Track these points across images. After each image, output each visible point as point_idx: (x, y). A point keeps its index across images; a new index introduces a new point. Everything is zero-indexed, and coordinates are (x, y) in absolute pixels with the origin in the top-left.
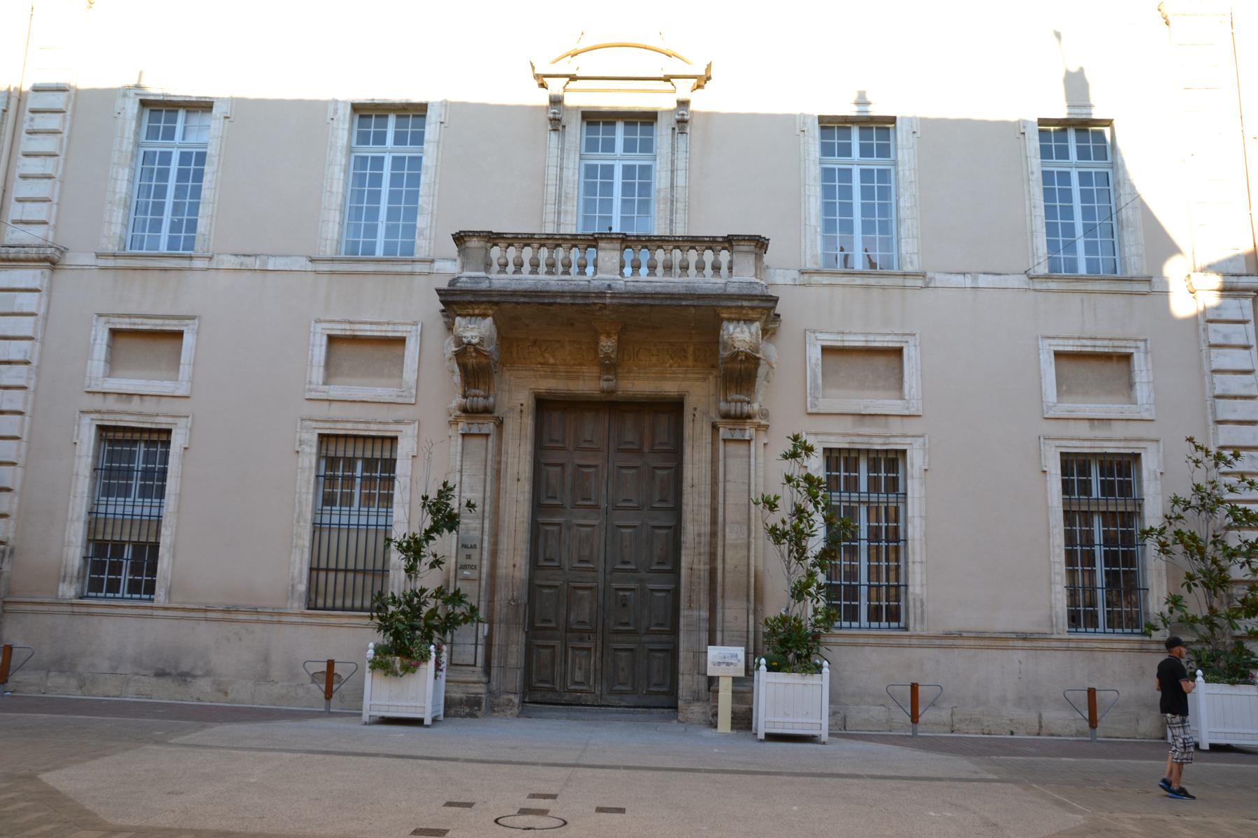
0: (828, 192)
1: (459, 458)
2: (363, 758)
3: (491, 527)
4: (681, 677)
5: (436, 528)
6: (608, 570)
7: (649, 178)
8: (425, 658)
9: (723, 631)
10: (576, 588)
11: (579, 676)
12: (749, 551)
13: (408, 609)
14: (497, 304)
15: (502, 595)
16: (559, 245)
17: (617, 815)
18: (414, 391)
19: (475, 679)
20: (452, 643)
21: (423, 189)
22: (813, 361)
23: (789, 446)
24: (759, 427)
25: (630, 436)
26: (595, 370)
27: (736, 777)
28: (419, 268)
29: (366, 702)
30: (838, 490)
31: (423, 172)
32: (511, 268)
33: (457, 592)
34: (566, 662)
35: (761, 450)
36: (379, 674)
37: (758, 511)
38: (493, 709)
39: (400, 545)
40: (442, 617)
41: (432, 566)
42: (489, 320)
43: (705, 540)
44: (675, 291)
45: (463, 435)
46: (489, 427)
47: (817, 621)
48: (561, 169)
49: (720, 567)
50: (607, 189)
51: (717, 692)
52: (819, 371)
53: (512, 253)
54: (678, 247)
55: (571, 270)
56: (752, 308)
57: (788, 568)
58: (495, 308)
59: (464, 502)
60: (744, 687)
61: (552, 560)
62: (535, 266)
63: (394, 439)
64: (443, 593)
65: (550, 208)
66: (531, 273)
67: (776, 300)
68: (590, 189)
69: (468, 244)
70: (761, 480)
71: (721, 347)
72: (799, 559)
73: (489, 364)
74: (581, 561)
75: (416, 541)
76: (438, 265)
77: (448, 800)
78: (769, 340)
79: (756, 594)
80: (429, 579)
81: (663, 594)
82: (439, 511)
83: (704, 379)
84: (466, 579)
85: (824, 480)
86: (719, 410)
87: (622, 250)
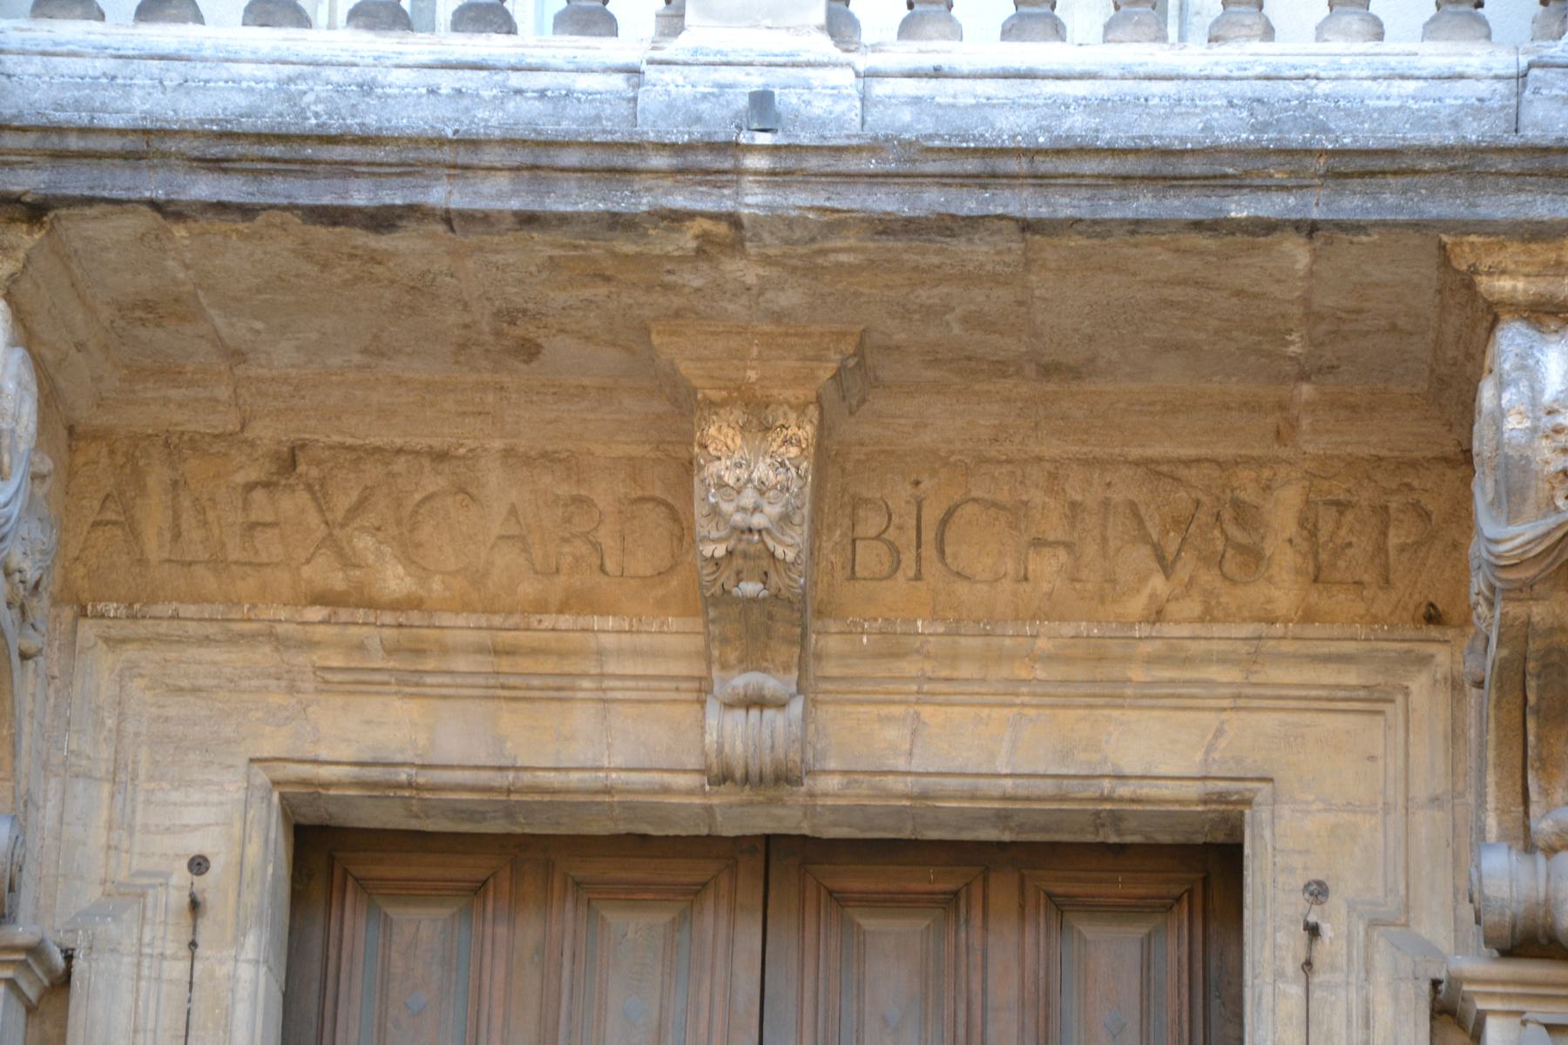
26: (676, 639)
44: (1183, 129)
71: (1484, 490)
83: (1373, 699)
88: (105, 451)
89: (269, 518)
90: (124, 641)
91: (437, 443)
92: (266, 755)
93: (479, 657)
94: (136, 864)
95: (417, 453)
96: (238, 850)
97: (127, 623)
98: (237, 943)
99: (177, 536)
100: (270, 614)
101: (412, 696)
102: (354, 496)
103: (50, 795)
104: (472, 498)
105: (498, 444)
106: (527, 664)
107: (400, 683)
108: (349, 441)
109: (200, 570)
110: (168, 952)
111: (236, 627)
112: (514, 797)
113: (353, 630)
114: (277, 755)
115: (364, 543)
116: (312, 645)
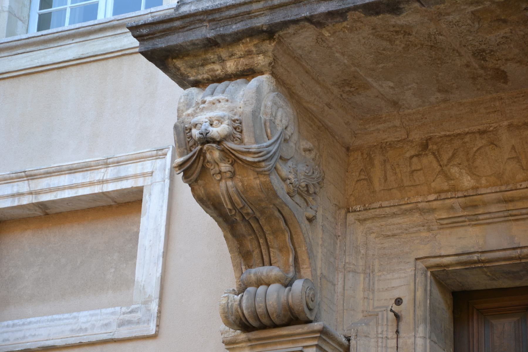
14: (270, 33)
18: (154, 307)
42: (263, 81)
58: (269, 46)
88: (360, 154)
89: (419, 168)
90: (365, 220)
91: (481, 128)
92: (421, 256)
93: (499, 205)
94: (376, 304)
95: (473, 133)
96: (413, 294)
97: (364, 212)
98: (415, 330)
99: (386, 180)
100: (415, 200)
101: (475, 225)
102: (450, 154)
103: (340, 279)
104: (496, 146)
105: (506, 123)
106: (519, 205)
107: (470, 220)
108: (448, 133)
109: (394, 191)
110: (389, 337)
111: (404, 207)
112: (523, 261)
113: (447, 201)
114: (425, 256)
115: (455, 171)
116: (433, 210)
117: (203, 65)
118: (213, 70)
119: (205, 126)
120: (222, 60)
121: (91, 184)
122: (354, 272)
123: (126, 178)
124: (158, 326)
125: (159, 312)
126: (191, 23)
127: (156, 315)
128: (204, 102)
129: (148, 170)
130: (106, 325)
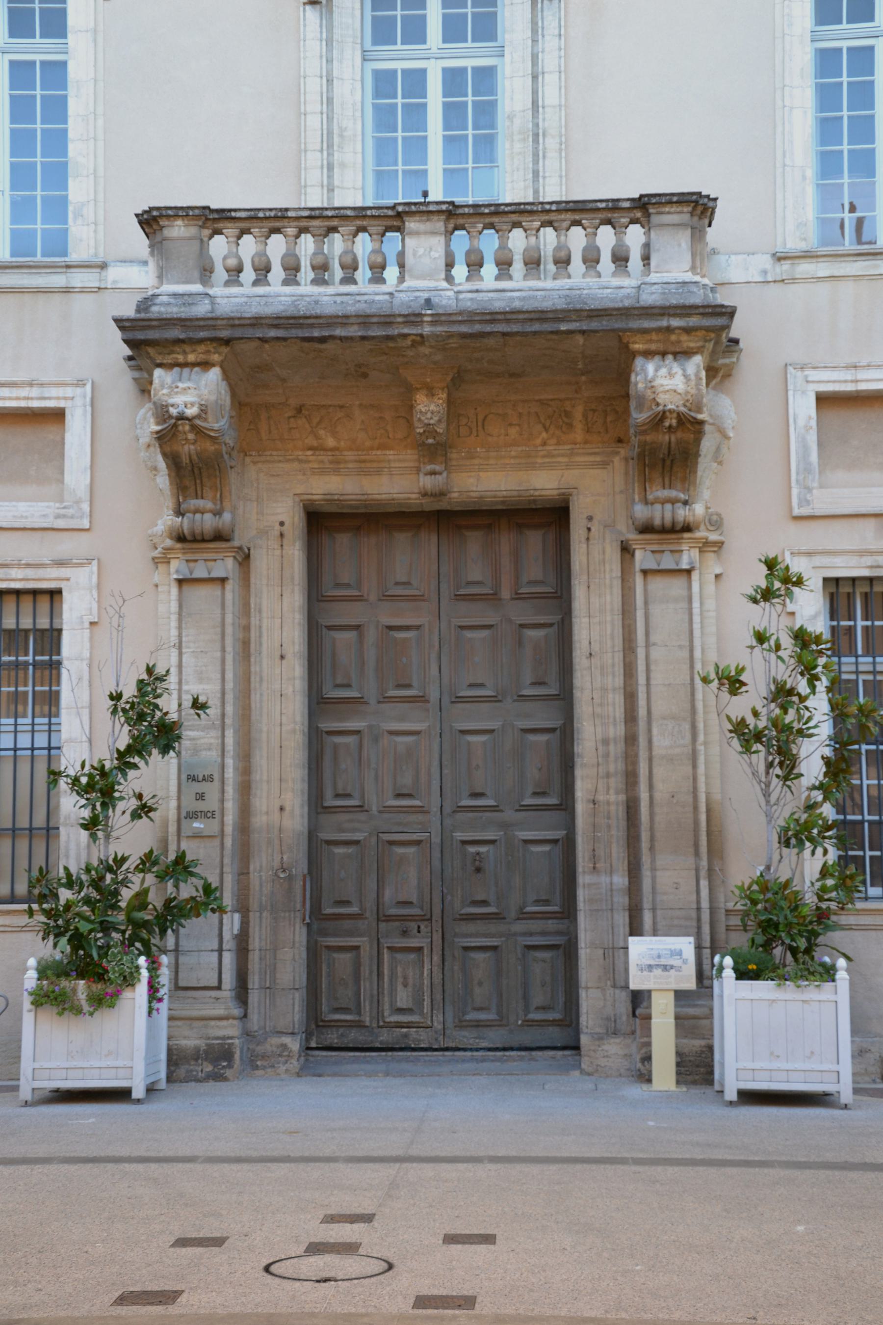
0: (827, 97)
1: (174, 623)
2: (22, 1168)
3: (237, 743)
4: (583, 994)
5: (137, 748)
6: (447, 809)
7: (492, 91)
8: (129, 980)
9: (654, 910)
10: (392, 843)
11: (403, 998)
12: (695, 766)
13: (94, 894)
14: (227, 342)
15: (263, 864)
16: (334, 229)
17: (482, 1248)
18: (86, 507)
19: (220, 1011)
20: (176, 950)
21: (75, 127)
22: (801, 422)
23: (759, 577)
24: (705, 546)
25: (476, 571)
26: (410, 456)
27: (689, 1172)
28: (79, 279)
29: (26, 1065)
30: (852, 652)
31: (71, 92)
32: (248, 275)
33: (180, 859)
34: (380, 974)
35: (711, 588)
36: (48, 1015)
37: (708, 696)
38: (255, 1063)
39: (76, 780)
40: (159, 905)
41: (136, 815)
42: (215, 374)
43: (616, 749)
44: (547, 305)
45: (180, 582)
46: (225, 566)
47: (824, 889)
48: (330, 81)
49: (644, 796)
50: (416, 115)
51: (649, 1017)
52: (812, 438)
53: (248, 246)
54: (550, 224)
55: (358, 275)
56: (688, 330)
57: (767, 795)
58: (225, 350)
59: (187, 702)
60: (695, 1007)
61: (348, 796)
62: (292, 269)
63: (55, 594)
64: (155, 863)
65: (314, 159)
66: (286, 282)
67: (730, 313)
68: (384, 118)
69: (166, 232)
70: (712, 641)
71: (633, 404)
72: (786, 778)
73: (219, 455)
74: (399, 796)
75: (103, 772)
76: (115, 274)
77: (178, 1234)
78: (718, 388)
79: (710, 842)
80: (131, 839)
81: (546, 848)
82: (141, 717)
83: (604, 464)
84: (197, 836)
85: (827, 636)
86: (632, 517)
87: (449, 233)
90: (258, 462)
91: (341, 403)
95: (335, 406)
99: (270, 432)
102: (318, 419)
105: (357, 403)
106: (368, 465)
115: (322, 432)
116: (309, 462)
117: (169, 354)
118: (177, 359)
119: (182, 407)
120: (185, 353)
121: (18, 398)
122: (250, 500)
123: (50, 398)
124: (90, 522)
125: (91, 512)
126: (166, 325)
127: (88, 514)
128: (177, 387)
129: (70, 395)
130: (44, 516)
